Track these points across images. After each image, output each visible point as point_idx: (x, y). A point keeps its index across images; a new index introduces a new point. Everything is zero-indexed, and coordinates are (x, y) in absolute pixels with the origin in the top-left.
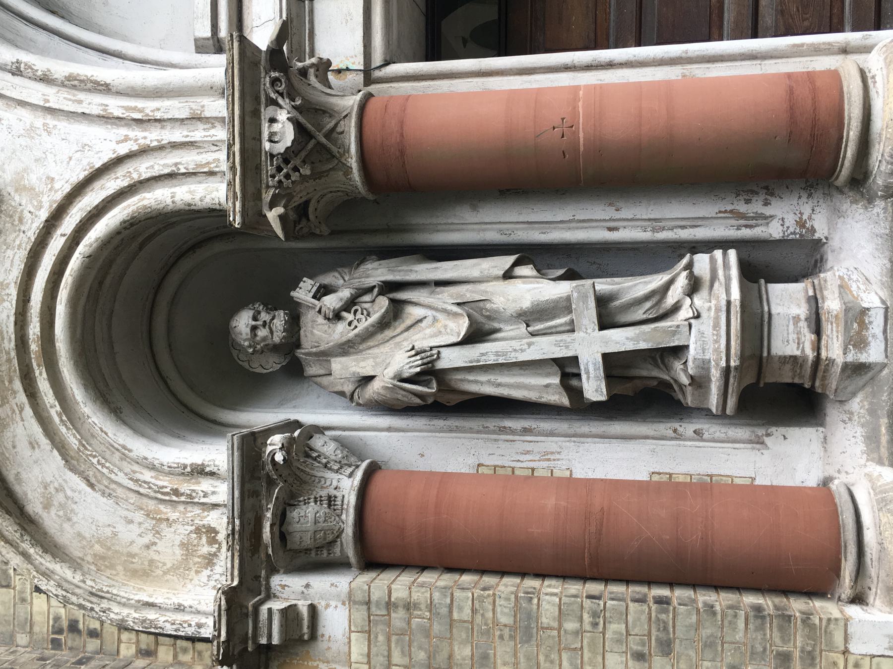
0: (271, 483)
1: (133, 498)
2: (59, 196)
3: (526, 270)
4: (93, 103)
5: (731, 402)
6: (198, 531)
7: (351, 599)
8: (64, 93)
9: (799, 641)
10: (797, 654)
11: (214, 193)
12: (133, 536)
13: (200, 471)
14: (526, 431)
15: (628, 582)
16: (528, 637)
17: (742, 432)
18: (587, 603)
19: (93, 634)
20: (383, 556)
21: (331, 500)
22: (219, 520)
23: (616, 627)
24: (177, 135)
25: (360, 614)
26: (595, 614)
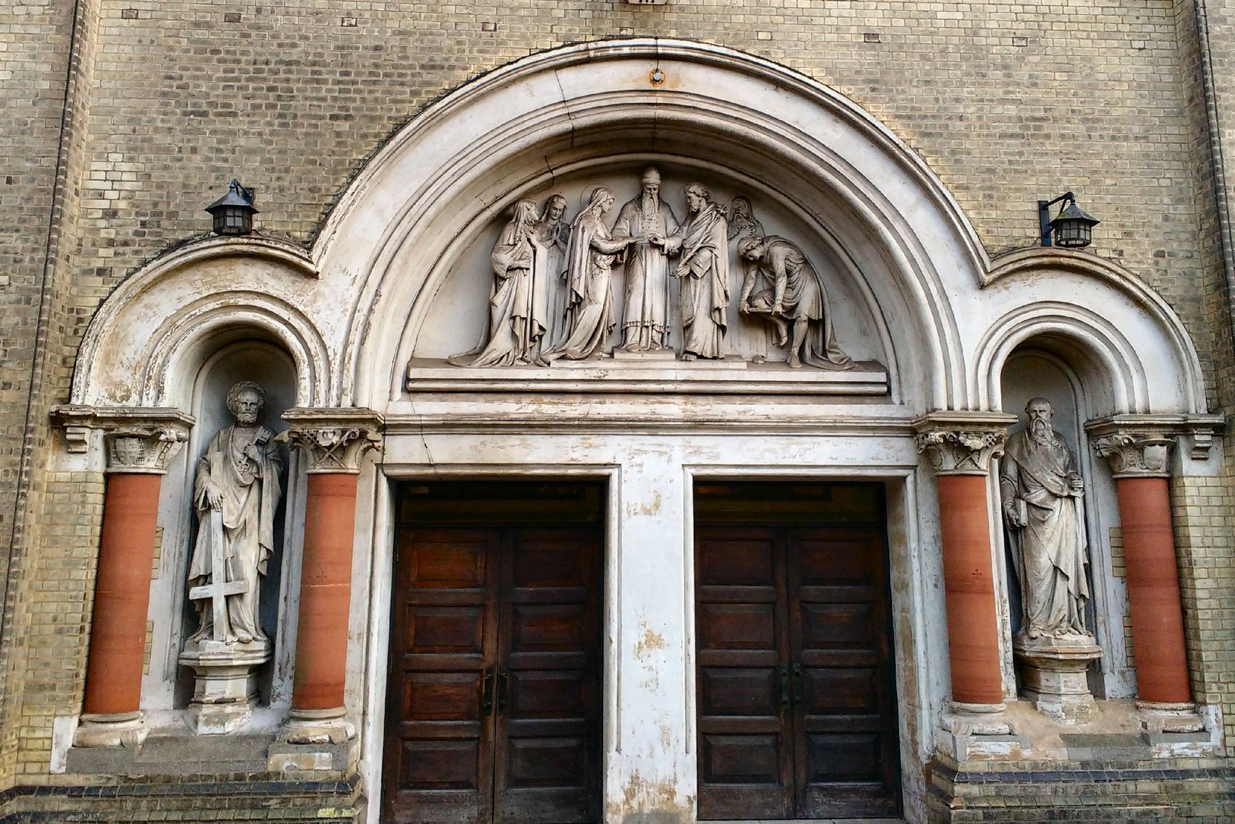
0: (151, 430)
1: (148, 353)
2: (309, 316)
3: (263, 554)
4: (356, 337)
5: (185, 662)
6: (128, 390)
7: (88, 472)
8: (362, 319)
9: (60, 694)
10: (54, 693)
11: (304, 403)
12: (127, 354)
13: (160, 391)
14: (181, 554)
15: (93, 612)
16: (66, 564)
17: (173, 669)
18: (82, 594)
19: (76, 332)
20: (112, 482)
21: (141, 459)
22: (132, 402)
23: (69, 607)
24: (335, 381)
25: (81, 478)
26: (76, 597)
